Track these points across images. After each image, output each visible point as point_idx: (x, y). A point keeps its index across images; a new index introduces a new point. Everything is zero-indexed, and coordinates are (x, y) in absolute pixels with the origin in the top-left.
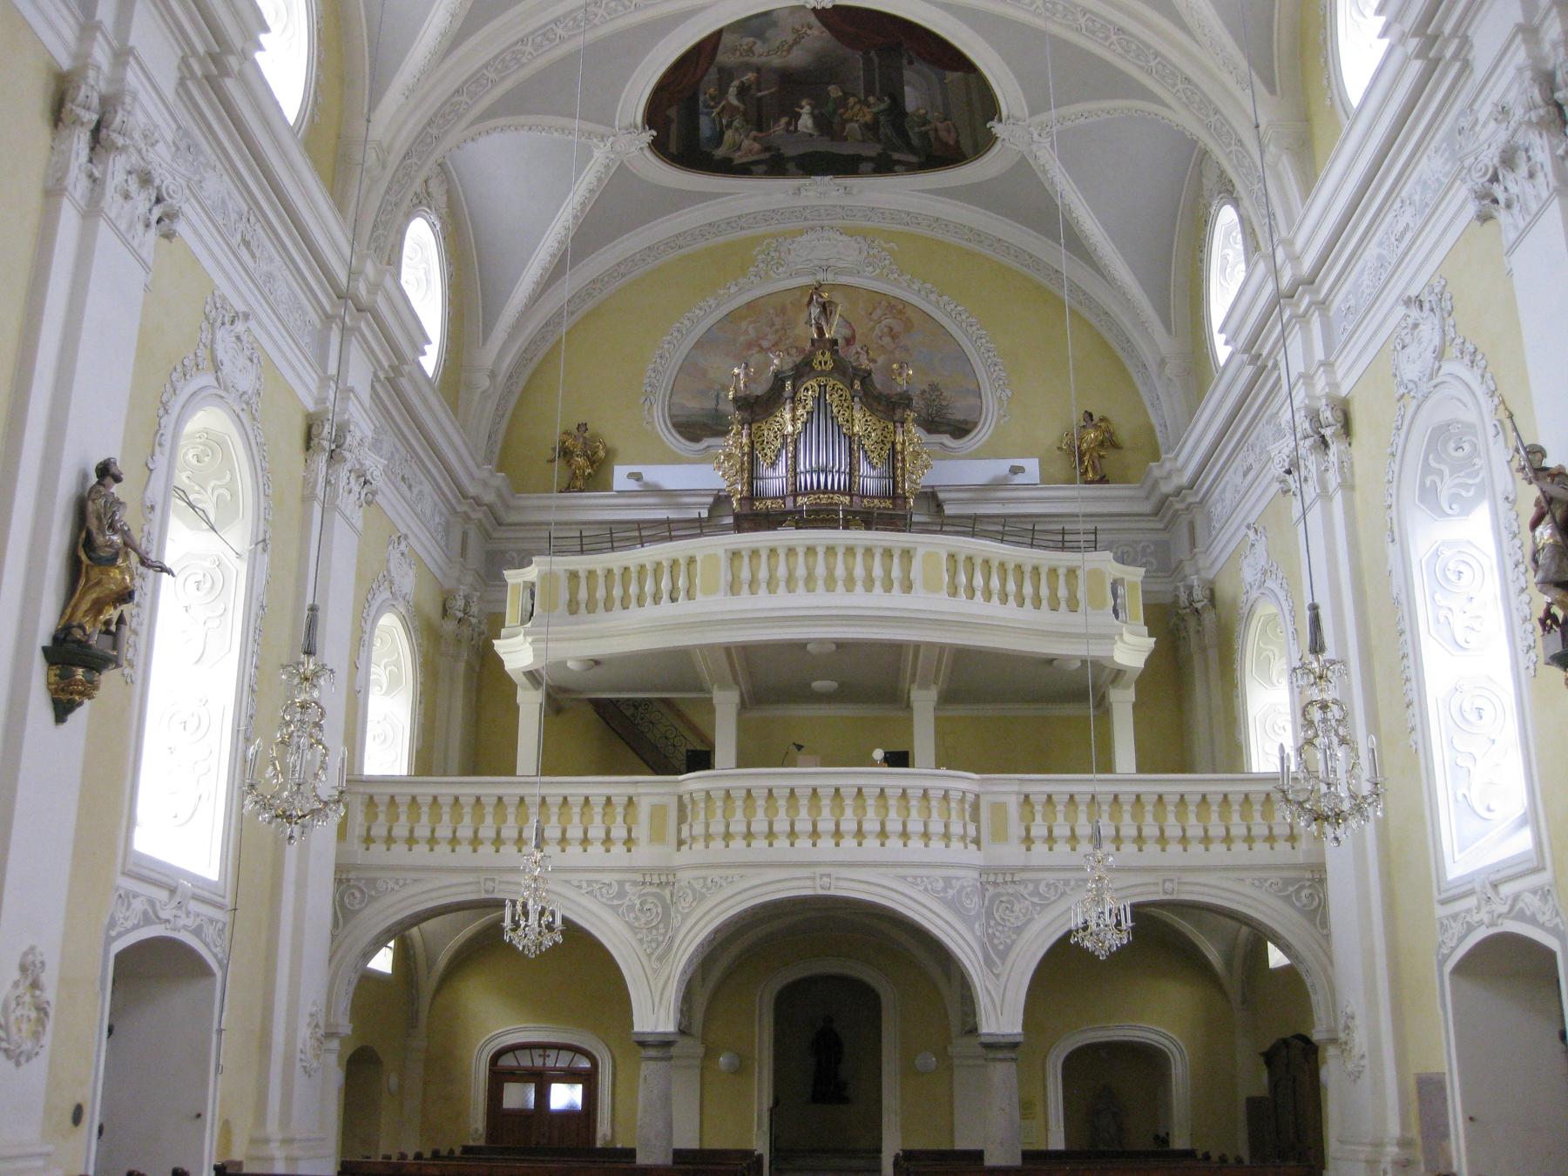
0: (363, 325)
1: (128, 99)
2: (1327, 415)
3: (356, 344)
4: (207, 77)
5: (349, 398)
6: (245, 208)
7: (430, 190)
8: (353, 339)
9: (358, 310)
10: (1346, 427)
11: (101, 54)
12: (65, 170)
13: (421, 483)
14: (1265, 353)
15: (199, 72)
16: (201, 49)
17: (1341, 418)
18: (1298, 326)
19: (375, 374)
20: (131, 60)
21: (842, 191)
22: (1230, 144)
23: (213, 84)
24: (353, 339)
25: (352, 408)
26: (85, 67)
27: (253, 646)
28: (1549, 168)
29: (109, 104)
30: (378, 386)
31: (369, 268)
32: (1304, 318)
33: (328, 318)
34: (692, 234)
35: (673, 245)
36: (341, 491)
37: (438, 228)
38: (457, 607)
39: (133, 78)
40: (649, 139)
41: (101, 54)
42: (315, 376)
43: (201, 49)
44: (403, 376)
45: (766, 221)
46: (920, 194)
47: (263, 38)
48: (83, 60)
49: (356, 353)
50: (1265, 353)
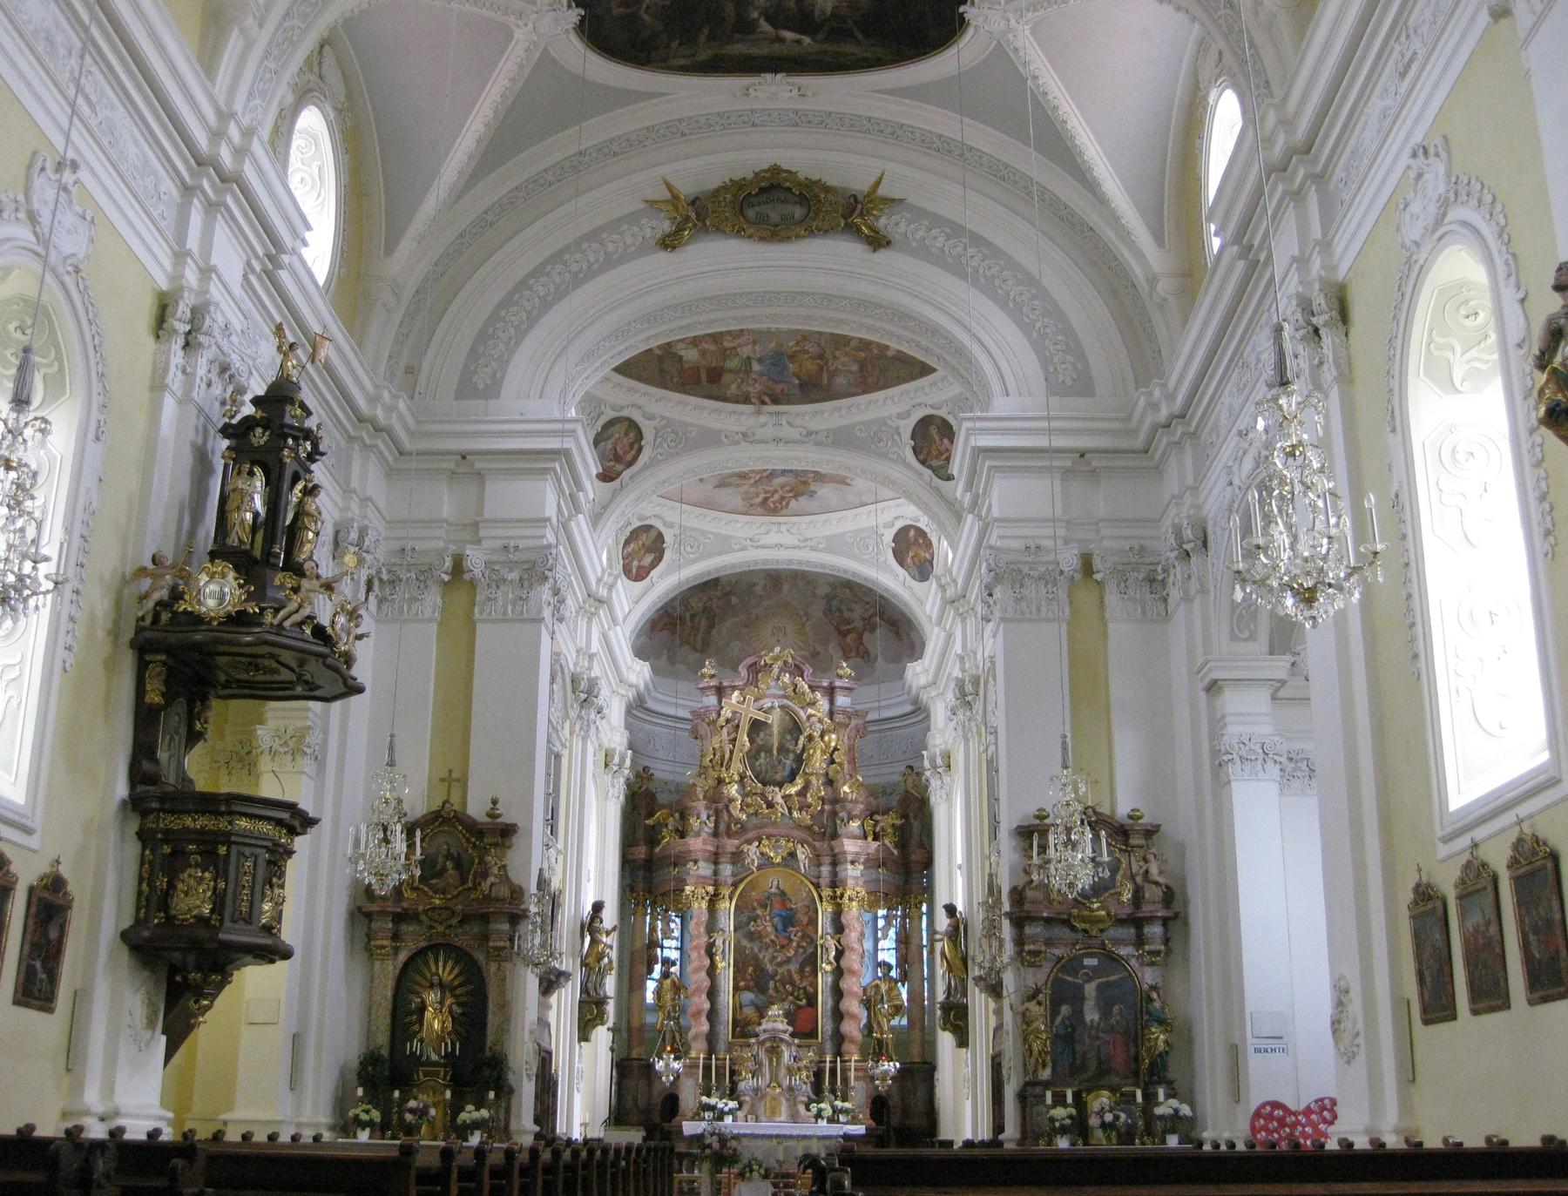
0: (230, 201)
1: (212, 308)
2: (1319, 301)
3: (223, 222)
4: (265, 271)
5: (210, 278)
6: (78, 44)
7: (323, 73)
8: (219, 216)
9: (376, 430)
10: (1343, 314)
11: (191, 276)
12: (166, 370)
13: (113, 108)
14: (1256, 243)
15: (258, 268)
16: (261, 252)
17: (1336, 305)
18: (1292, 205)
19: (248, 264)
20: (213, 275)
21: (795, 92)
22: (1219, 9)
23: (271, 277)
24: (219, 216)
25: (212, 288)
26: (182, 288)
27: (324, 745)
28: (1307, 372)
29: (198, 315)
30: (252, 278)
31: (386, 395)
32: (1298, 196)
33: (188, 190)
34: (627, 140)
35: (606, 151)
36: (198, 381)
37: (332, 118)
38: (350, 539)
39: (215, 291)
40: (576, 20)
41: (191, 276)
42: (169, 251)
43: (261, 252)
44: (282, 268)
45: (710, 126)
46: (876, 95)
47: (308, 235)
48: (177, 277)
49: (222, 233)
50: (1256, 243)
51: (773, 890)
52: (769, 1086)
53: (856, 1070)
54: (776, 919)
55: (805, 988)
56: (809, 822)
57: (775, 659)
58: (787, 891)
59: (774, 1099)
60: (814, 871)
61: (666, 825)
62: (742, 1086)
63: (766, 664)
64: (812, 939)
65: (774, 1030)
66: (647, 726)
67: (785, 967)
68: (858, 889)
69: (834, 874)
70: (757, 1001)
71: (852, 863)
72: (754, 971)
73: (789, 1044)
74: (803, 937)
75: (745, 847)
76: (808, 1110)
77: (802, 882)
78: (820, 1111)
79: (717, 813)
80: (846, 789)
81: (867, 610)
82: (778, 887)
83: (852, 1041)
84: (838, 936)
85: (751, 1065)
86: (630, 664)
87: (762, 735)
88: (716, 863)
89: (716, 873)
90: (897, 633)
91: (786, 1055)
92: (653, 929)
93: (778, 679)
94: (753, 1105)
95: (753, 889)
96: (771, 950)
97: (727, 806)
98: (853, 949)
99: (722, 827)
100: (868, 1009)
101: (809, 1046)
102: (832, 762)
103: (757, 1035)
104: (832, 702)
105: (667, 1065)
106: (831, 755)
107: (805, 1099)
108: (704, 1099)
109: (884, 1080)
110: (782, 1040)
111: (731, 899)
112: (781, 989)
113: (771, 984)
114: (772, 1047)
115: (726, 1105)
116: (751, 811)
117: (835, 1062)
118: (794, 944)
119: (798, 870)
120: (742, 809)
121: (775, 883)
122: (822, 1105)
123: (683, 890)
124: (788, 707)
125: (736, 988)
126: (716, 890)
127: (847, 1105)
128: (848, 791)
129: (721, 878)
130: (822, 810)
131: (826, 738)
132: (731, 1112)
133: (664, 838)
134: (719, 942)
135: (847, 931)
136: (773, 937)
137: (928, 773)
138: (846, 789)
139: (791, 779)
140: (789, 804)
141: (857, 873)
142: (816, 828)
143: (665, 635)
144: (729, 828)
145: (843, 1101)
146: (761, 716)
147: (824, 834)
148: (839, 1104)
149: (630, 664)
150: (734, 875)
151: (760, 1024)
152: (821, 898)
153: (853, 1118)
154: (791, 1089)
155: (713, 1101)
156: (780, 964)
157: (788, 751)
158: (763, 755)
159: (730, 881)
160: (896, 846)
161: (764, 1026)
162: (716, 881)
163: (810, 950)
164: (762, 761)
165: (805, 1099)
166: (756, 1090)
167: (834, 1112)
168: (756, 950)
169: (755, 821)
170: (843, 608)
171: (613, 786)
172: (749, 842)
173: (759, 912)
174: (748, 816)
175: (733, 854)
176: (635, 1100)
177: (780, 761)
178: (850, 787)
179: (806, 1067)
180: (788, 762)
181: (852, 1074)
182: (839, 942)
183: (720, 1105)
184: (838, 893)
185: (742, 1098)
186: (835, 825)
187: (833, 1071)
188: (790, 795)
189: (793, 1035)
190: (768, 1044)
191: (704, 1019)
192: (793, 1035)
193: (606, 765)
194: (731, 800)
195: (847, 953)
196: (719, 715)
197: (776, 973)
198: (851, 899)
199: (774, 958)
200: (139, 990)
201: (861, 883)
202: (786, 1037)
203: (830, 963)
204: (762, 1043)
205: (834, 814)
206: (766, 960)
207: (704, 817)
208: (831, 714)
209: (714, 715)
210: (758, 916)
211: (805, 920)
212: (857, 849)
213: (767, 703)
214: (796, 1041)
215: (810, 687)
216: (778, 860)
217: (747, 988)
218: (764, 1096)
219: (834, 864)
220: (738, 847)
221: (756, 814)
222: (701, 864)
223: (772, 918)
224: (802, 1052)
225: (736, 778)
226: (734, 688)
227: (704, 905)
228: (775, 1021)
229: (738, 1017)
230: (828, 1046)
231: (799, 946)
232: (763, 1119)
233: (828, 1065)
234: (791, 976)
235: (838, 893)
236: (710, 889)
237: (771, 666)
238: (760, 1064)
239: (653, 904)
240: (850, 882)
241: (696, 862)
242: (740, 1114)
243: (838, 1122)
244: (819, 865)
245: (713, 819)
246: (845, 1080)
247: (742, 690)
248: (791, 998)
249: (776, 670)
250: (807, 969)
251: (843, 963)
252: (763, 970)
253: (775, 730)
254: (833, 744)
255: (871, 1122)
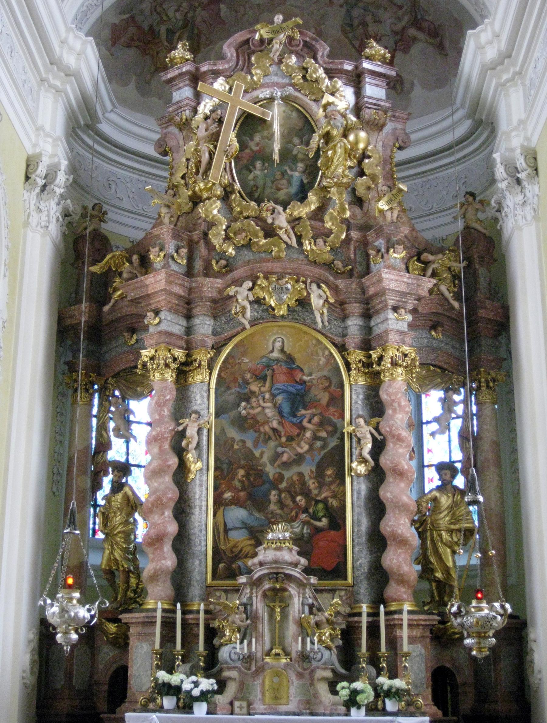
51: (276, 355)
52: (268, 654)
53: (410, 626)
54: (280, 399)
55: (325, 501)
56: (328, 257)
57: (276, 32)
58: (297, 356)
59: (278, 674)
60: (335, 328)
61: (120, 274)
62: (224, 653)
63: (262, 40)
64: (334, 425)
65: (276, 562)
66: (108, 167)
67: (295, 469)
68: (406, 349)
69: (368, 329)
70: (252, 522)
71: (395, 309)
72: (247, 475)
73: (301, 585)
74: (321, 424)
75: (232, 291)
76: (335, 692)
77: (319, 342)
78: (355, 693)
79: (192, 246)
80: (383, 205)
81: (399, 19)
82: (282, 351)
83: (402, 581)
84: (375, 420)
85: (238, 618)
86: (63, 34)
87: (257, 138)
88: (189, 317)
89: (189, 330)
90: (441, 47)
91: (296, 603)
92: (102, 427)
93: (280, 62)
94: (242, 685)
95: (244, 354)
96: (272, 444)
97: (206, 234)
98: (399, 439)
99: (198, 265)
100: (421, 535)
101: (333, 591)
102: (362, 173)
103: (249, 572)
104: (358, 93)
105: (64, 611)
106: (360, 162)
107: (329, 674)
108: (163, 676)
109: (481, 636)
110: (289, 577)
111: (211, 368)
112: (289, 502)
113: (273, 496)
114: (273, 590)
115: (196, 684)
116: (240, 239)
117: (377, 614)
118: (308, 434)
119: (313, 325)
120: (227, 238)
121: (278, 345)
122: (358, 685)
123: (139, 356)
124: (295, 100)
125: (218, 502)
126: (188, 355)
127: (399, 683)
128: (386, 207)
129: (197, 337)
130: (348, 240)
131: (352, 137)
132: (204, 696)
133: (115, 290)
134: (192, 431)
135: (390, 412)
136: (275, 424)
137: (502, 185)
138: (383, 205)
139: (302, 197)
140: (299, 229)
141: (404, 326)
142: (339, 264)
143: (132, 54)
144: (208, 267)
145: (390, 678)
146: (256, 111)
147: (351, 271)
148: (384, 681)
149: (63, 34)
150: (215, 333)
151: (255, 554)
152: (348, 365)
153: (409, 704)
154: (304, 657)
155: (175, 679)
156: (286, 465)
157: (295, 159)
158: (258, 164)
159: (210, 342)
160: (458, 297)
161: (261, 557)
162: (188, 342)
163: (333, 443)
164: (257, 172)
165: (329, 674)
166: (248, 659)
167: (377, 696)
168: (250, 444)
169: (247, 255)
170: (369, 19)
171: (39, 210)
172: (238, 283)
173: (254, 387)
174: (238, 248)
175: (214, 301)
176: (69, 675)
177: (284, 174)
178: (389, 202)
179: (329, 622)
180: (297, 174)
181: (405, 633)
182: (377, 429)
183: (187, 686)
184: (375, 355)
185: (226, 674)
186: (368, 255)
187: (373, 629)
188: (299, 219)
189: (307, 571)
190: (267, 585)
191: (167, 548)
192: (307, 571)
193: (27, 178)
194: (212, 224)
195: (390, 445)
196: (195, 111)
197: (281, 478)
198: (395, 364)
199: (277, 456)
200: (31, 630)
201: (409, 340)
202: (296, 573)
203: (365, 461)
204: (257, 583)
205: (365, 244)
206: (265, 459)
207: (170, 248)
208: (358, 109)
209: (187, 113)
210: (253, 393)
211: (325, 398)
212: (403, 288)
213: (265, 93)
214: (313, 580)
215: (327, 71)
216: (283, 311)
217: (236, 502)
218: (260, 670)
219: (367, 315)
220: (220, 291)
221: (248, 245)
222: (163, 315)
223: (273, 396)
224: (323, 599)
225: (219, 192)
226: (216, 74)
227: (170, 376)
228: (279, 549)
229: (222, 547)
230: (364, 590)
231: (315, 438)
232: (259, 706)
233: (365, 620)
234: (303, 482)
235: (375, 355)
236: (179, 354)
237: (270, 41)
238: (253, 617)
239: (102, 391)
240: (393, 337)
241: (157, 313)
242: (221, 700)
243: (384, 712)
244: (345, 318)
245: (184, 251)
246: (393, 643)
247: (228, 77)
248: (303, 516)
249: (277, 46)
250: (329, 472)
251: (385, 460)
252: (260, 474)
253: (276, 128)
254: (361, 146)
255: (434, 708)
